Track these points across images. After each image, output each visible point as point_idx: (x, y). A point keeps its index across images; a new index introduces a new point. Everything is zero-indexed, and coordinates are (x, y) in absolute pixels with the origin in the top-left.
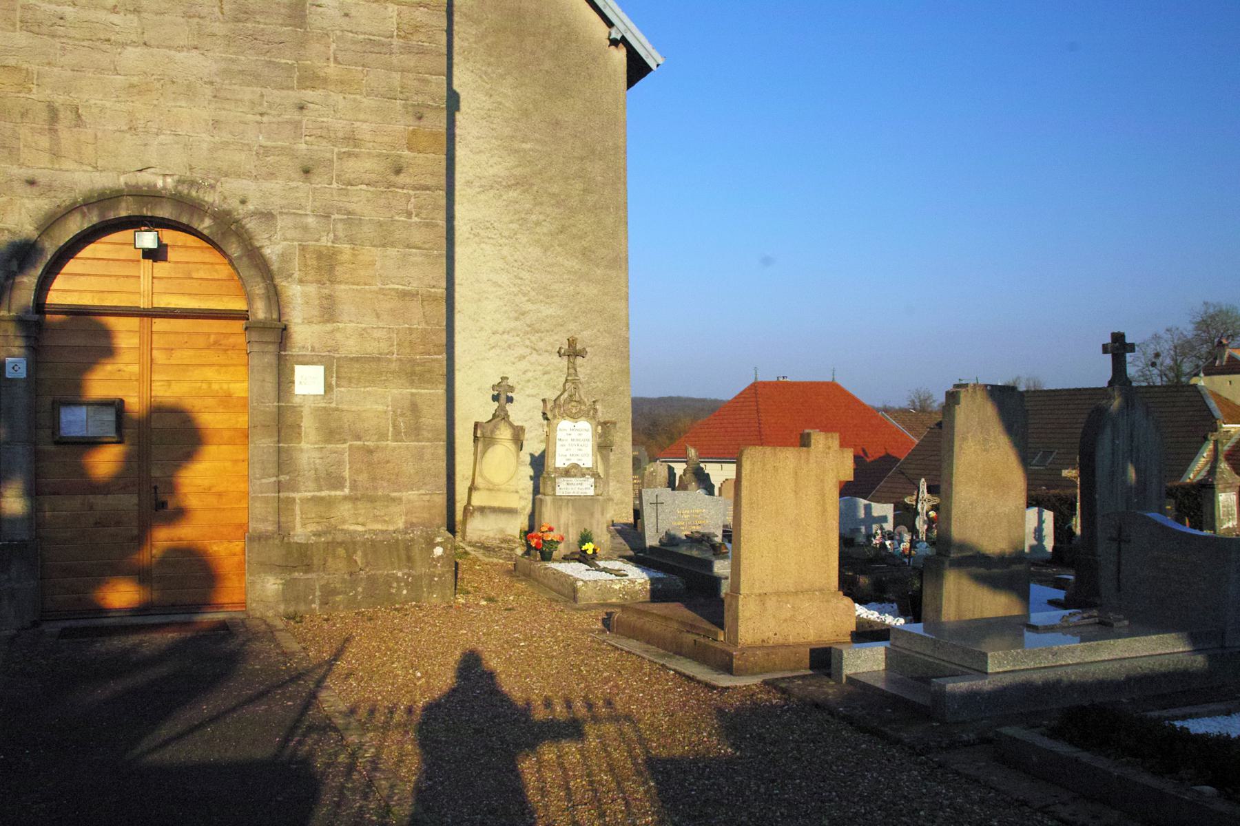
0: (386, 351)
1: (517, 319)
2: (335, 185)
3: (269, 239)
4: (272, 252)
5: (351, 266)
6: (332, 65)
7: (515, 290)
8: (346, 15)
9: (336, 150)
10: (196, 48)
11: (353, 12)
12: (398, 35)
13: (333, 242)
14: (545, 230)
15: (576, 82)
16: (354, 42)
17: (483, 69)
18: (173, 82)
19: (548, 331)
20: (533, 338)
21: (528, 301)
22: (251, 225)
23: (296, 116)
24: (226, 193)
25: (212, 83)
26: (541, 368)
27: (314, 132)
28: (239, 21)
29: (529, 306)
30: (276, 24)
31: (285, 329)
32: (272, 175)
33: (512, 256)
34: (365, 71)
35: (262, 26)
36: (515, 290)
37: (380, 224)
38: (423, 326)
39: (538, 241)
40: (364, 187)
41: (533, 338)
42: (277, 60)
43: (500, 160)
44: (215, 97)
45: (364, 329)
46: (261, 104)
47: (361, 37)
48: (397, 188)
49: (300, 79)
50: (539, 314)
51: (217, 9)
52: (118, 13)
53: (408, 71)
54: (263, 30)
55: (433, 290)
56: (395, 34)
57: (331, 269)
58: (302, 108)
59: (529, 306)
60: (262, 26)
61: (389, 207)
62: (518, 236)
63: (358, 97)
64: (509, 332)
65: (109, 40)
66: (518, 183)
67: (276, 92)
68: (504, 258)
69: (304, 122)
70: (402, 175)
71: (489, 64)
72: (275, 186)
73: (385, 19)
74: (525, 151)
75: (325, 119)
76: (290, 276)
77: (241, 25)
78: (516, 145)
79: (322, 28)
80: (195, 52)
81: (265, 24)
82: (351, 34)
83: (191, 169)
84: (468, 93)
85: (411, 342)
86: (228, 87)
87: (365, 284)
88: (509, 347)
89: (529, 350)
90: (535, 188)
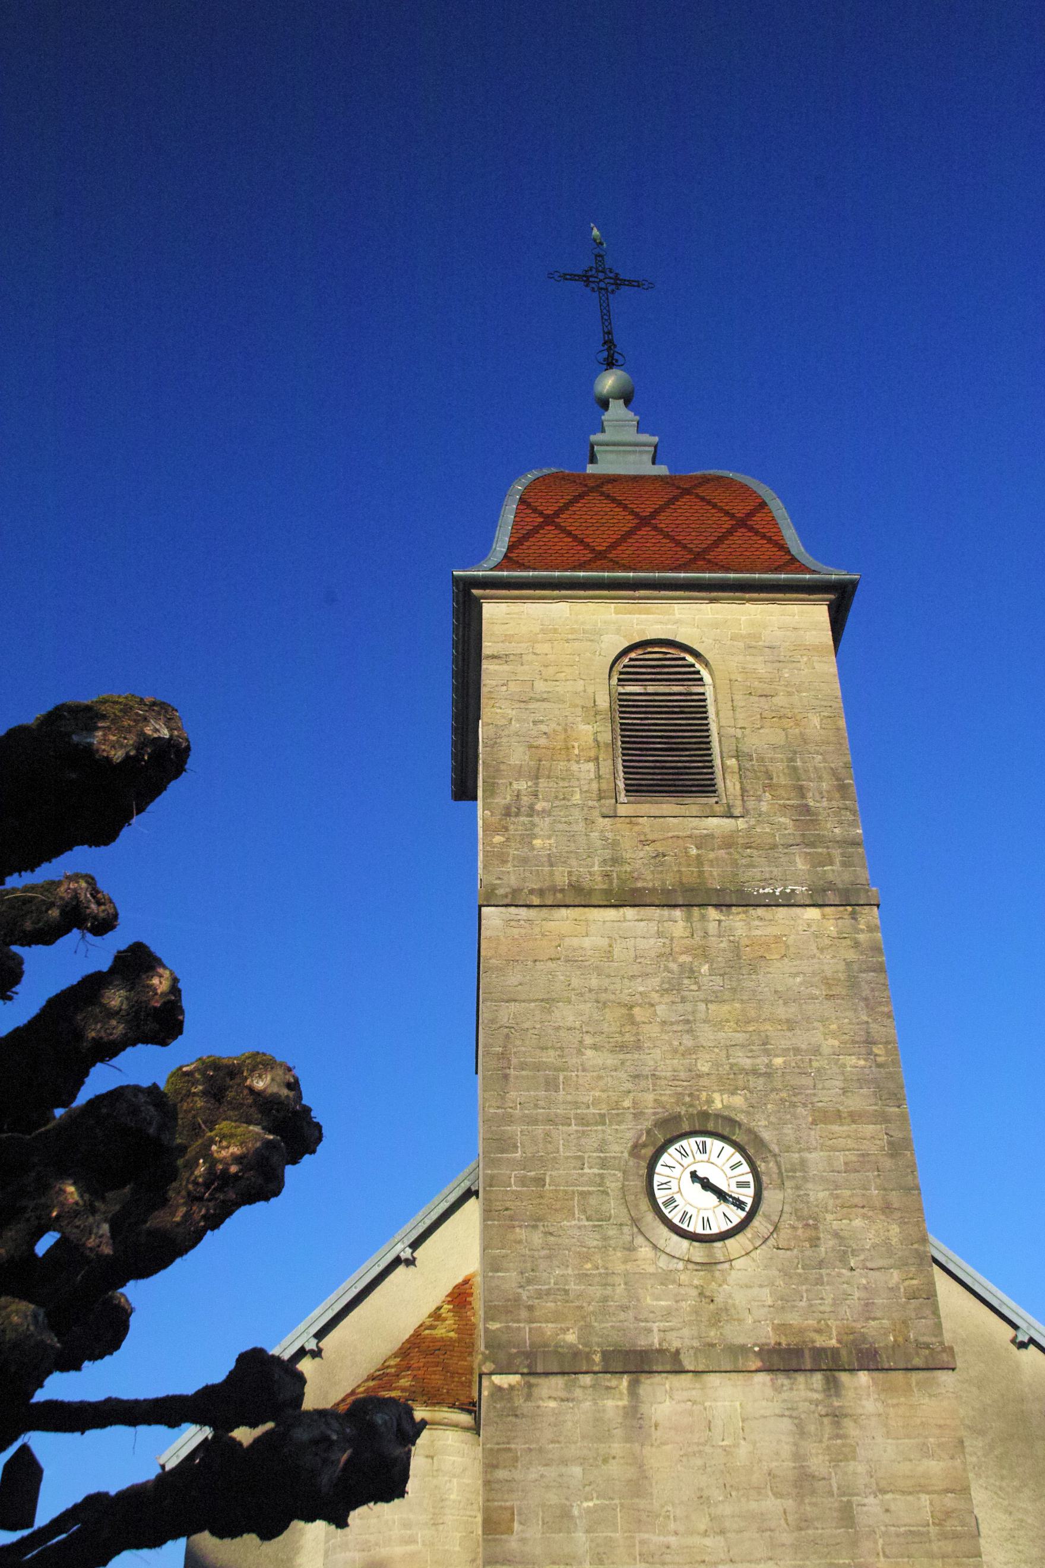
6: (882, 1559)
8: (887, 1511)
11: (893, 1507)
12: (933, 1523)
16: (898, 1535)
17: (997, 1483)
28: (801, 1529)
30: (831, 1527)
34: (911, 1563)
47: (902, 1529)
52: (709, 1536)
53: (948, 1557)
54: (821, 1534)
56: (931, 1522)
60: (820, 1531)
65: (704, 1562)
71: (1002, 1478)
77: (803, 1533)
79: (870, 1526)
80: (771, 1563)
81: (823, 1529)
82: (893, 1528)
84: (986, 1513)
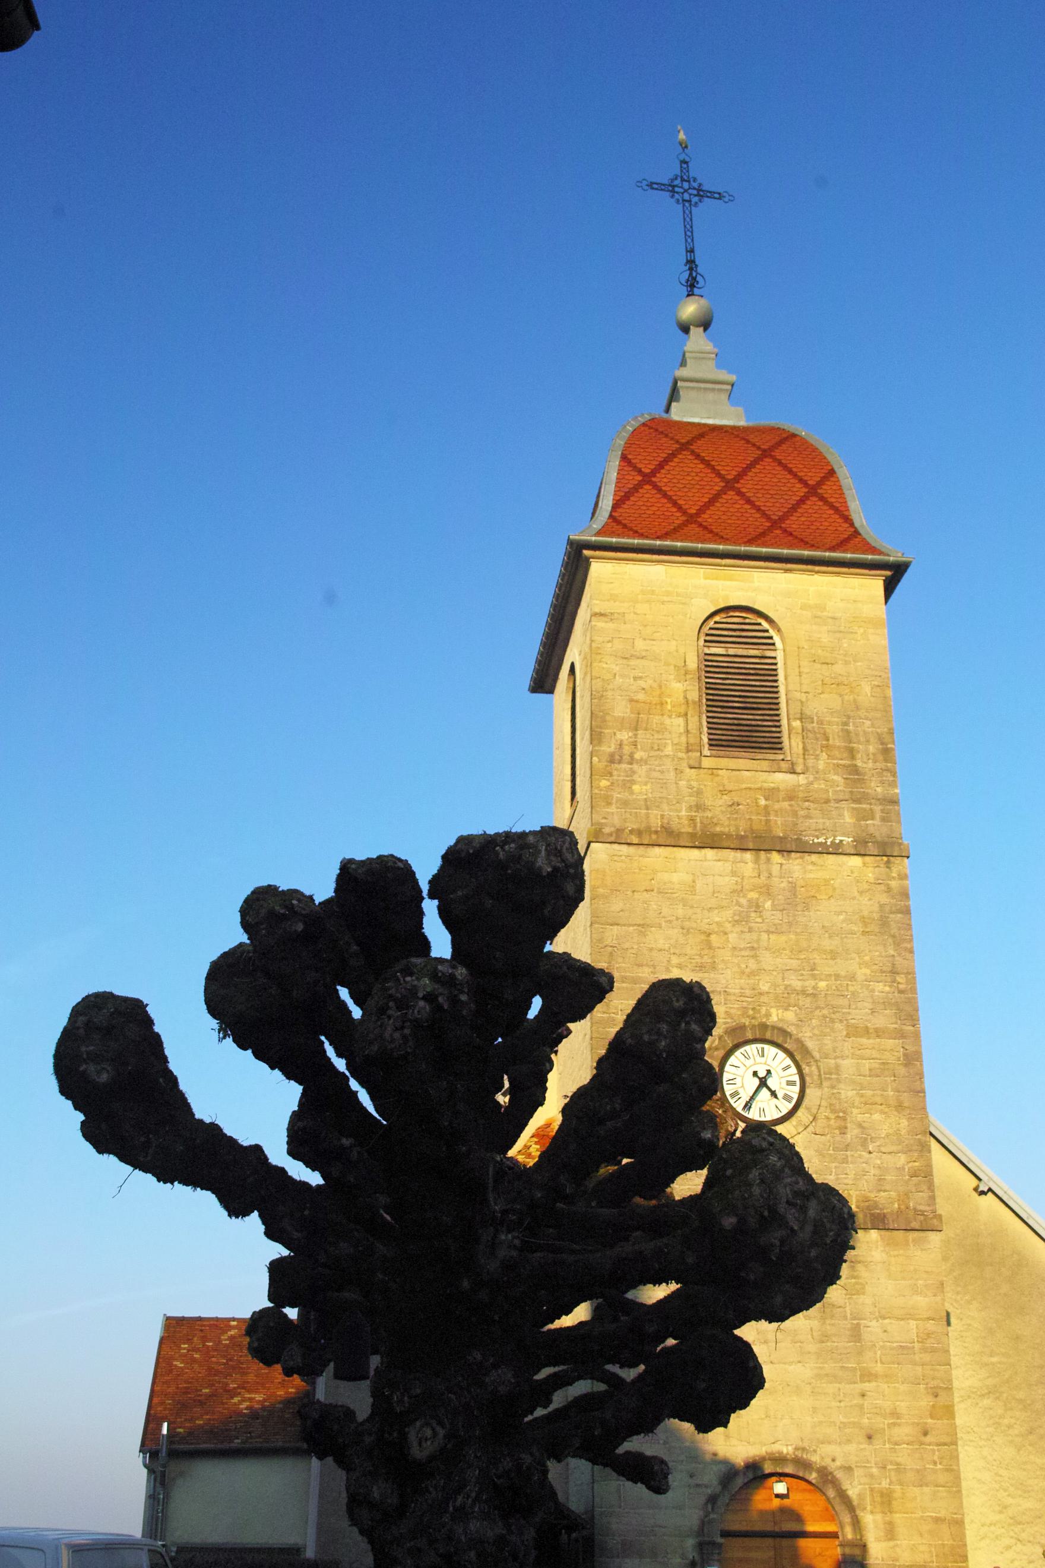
0: (929, 1560)
1: (1001, 1512)
2: (887, 1446)
3: (851, 1484)
4: (853, 1493)
5: (901, 1501)
6: (879, 1364)
7: (997, 1486)
8: (885, 1331)
9: (886, 1422)
10: (800, 1362)
12: (918, 1341)
13: (890, 1485)
14: (1016, 1432)
15: (1029, 1301)
16: (892, 1349)
18: (788, 1385)
19: (1028, 1523)
20: (1016, 1530)
21: (1009, 1495)
22: (839, 1475)
23: (859, 1401)
24: (823, 1455)
25: (810, 1384)
26: (1026, 1557)
27: (872, 1411)
28: (823, 1342)
29: (1010, 1501)
31: (865, 1546)
32: (849, 1441)
33: (991, 1455)
35: (836, 1344)
36: (997, 1486)
37: (918, 1471)
38: (951, 1542)
39: (1011, 1442)
40: (905, 1446)
41: (1016, 1530)
42: (846, 1365)
43: (973, 1373)
44: (812, 1392)
45: (914, 1545)
46: (839, 1395)
48: (926, 1445)
49: (862, 1376)
50: (1019, 1508)
51: (810, 1336)
54: (837, 1346)
55: (955, 1516)
57: (890, 1503)
58: (863, 1395)
59: (1010, 1501)
60: (836, 1344)
61: (922, 1459)
62: (995, 1438)
63: (896, 1385)
64: (995, 1525)
66: (990, 1392)
67: (847, 1386)
68: (985, 1458)
69: (866, 1405)
70: (929, 1436)
71: (958, 1293)
72: (851, 1448)
73: (909, 1331)
74: (993, 1364)
75: (878, 1402)
76: (865, 1509)
77: (824, 1344)
78: (985, 1359)
79: (872, 1342)
81: (838, 1342)
82: (889, 1344)
83: (802, 1440)
85: (944, 1554)
86: (819, 1385)
87: (912, 1513)
88: (997, 1537)
89: (1013, 1541)
90: (1005, 1395)
